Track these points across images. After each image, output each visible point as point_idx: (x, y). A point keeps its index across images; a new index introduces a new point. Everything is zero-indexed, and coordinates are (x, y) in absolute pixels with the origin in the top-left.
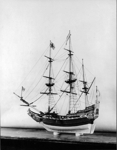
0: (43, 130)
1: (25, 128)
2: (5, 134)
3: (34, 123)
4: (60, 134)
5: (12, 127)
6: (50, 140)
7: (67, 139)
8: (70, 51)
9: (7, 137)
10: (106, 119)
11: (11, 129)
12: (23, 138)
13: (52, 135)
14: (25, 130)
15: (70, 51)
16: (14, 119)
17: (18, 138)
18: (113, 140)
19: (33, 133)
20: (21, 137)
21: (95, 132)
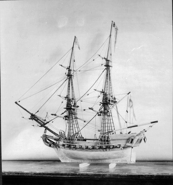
0: (56, 161)
1: (32, 160)
2: (7, 168)
3: (50, 152)
4: (118, 165)
5: (154, 160)
6: (79, 174)
7: (102, 172)
8: (107, 60)
9: (19, 173)
10: (159, 146)
11: (12, 163)
12: (41, 173)
13: (78, 168)
14: (38, 163)
15: (107, 60)
16: (25, 148)
17: (34, 174)
18: (168, 171)
19: (161, 167)
20: (38, 172)
21: (136, 161)
